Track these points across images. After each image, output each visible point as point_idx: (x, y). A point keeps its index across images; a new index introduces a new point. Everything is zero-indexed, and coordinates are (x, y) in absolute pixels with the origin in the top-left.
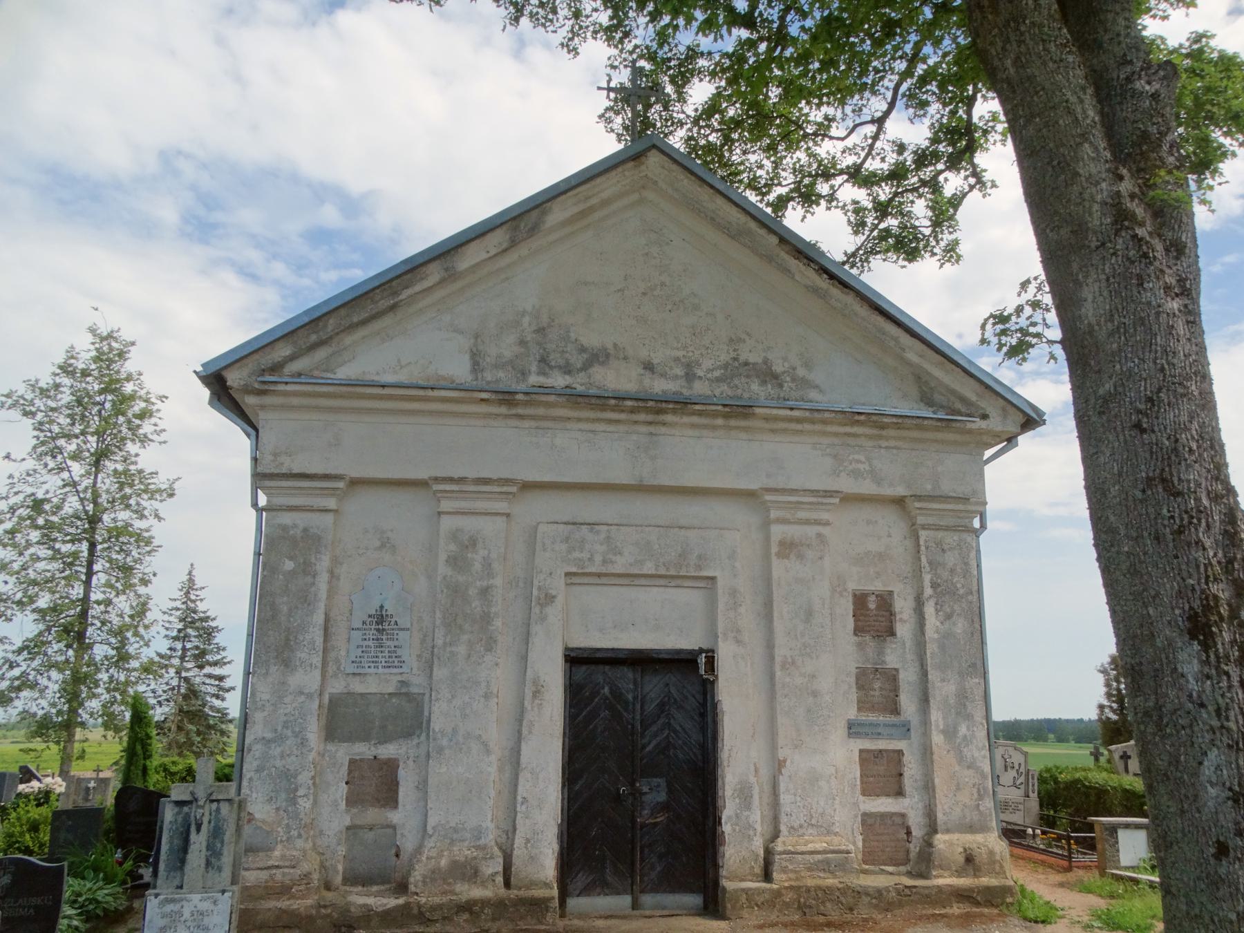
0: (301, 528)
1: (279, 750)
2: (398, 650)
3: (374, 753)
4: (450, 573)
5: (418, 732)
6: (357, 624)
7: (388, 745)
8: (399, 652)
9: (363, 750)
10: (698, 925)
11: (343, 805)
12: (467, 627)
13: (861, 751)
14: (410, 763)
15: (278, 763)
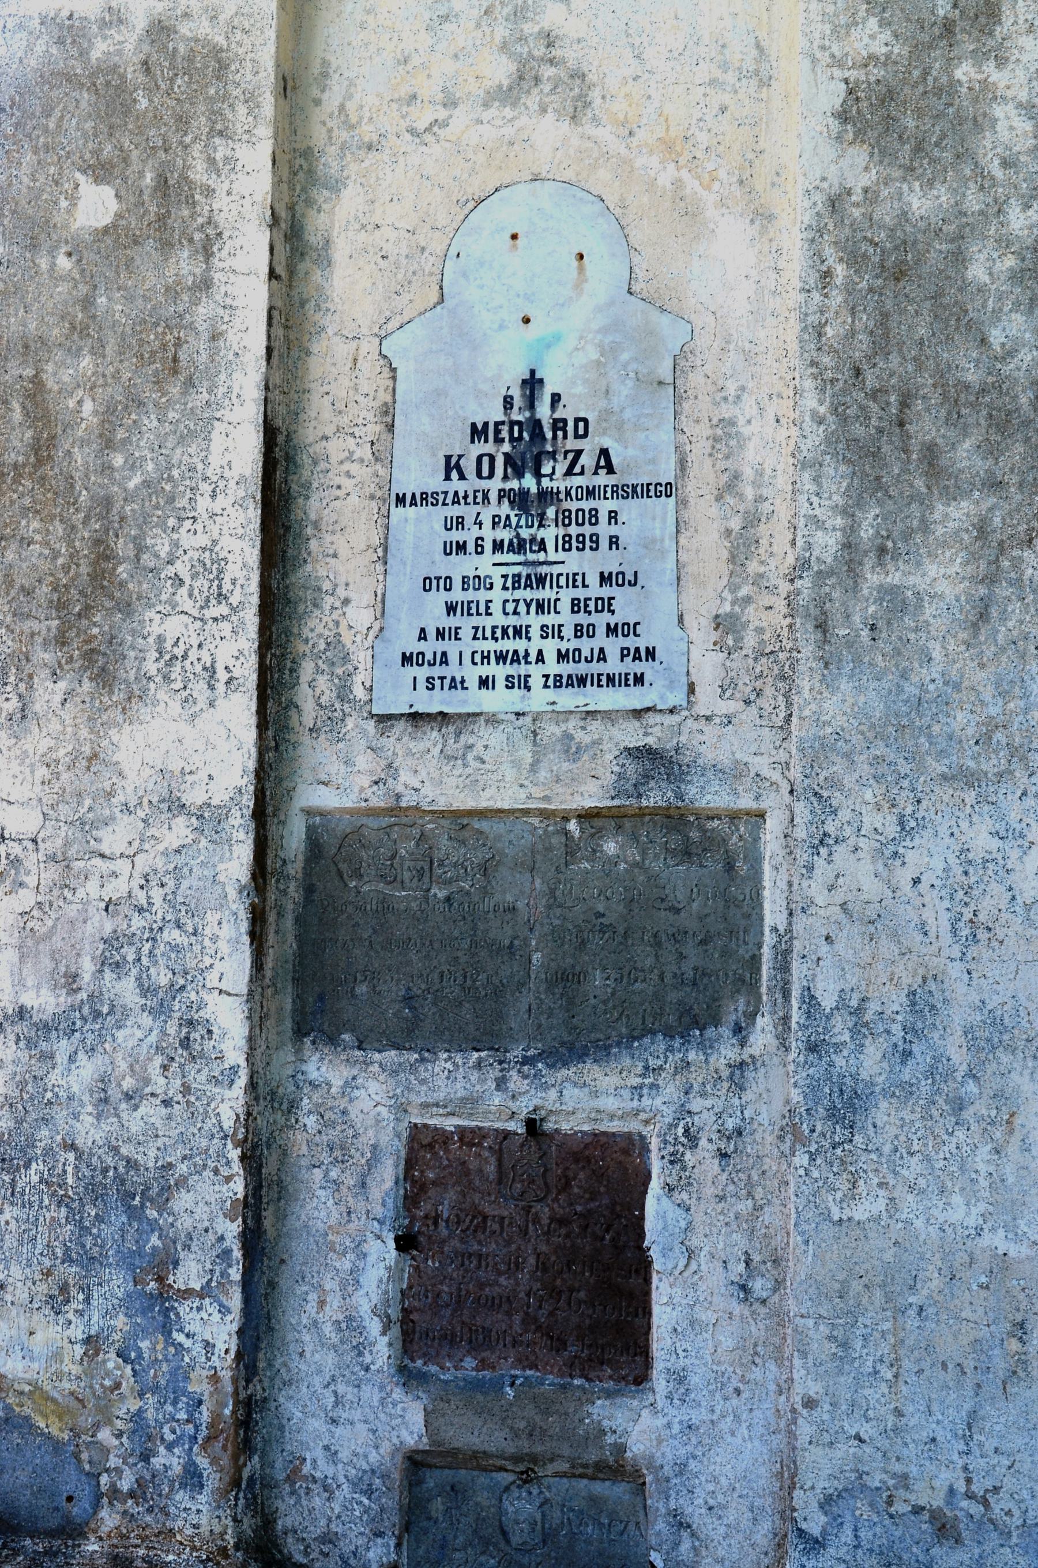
0: (141, 23)
1: (87, 1070)
2: (621, 596)
3: (524, 1106)
4: (860, 181)
5: (735, 1009)
6: (418, 473)
7: (591, 1071)
8: (626, 605)
9: (470, 1092)
10: (251, 99)
11: (382, 1350)
12: (965, 455)
13: (422, 1145)
14: (703, 1160)
15: (89, 1131)
